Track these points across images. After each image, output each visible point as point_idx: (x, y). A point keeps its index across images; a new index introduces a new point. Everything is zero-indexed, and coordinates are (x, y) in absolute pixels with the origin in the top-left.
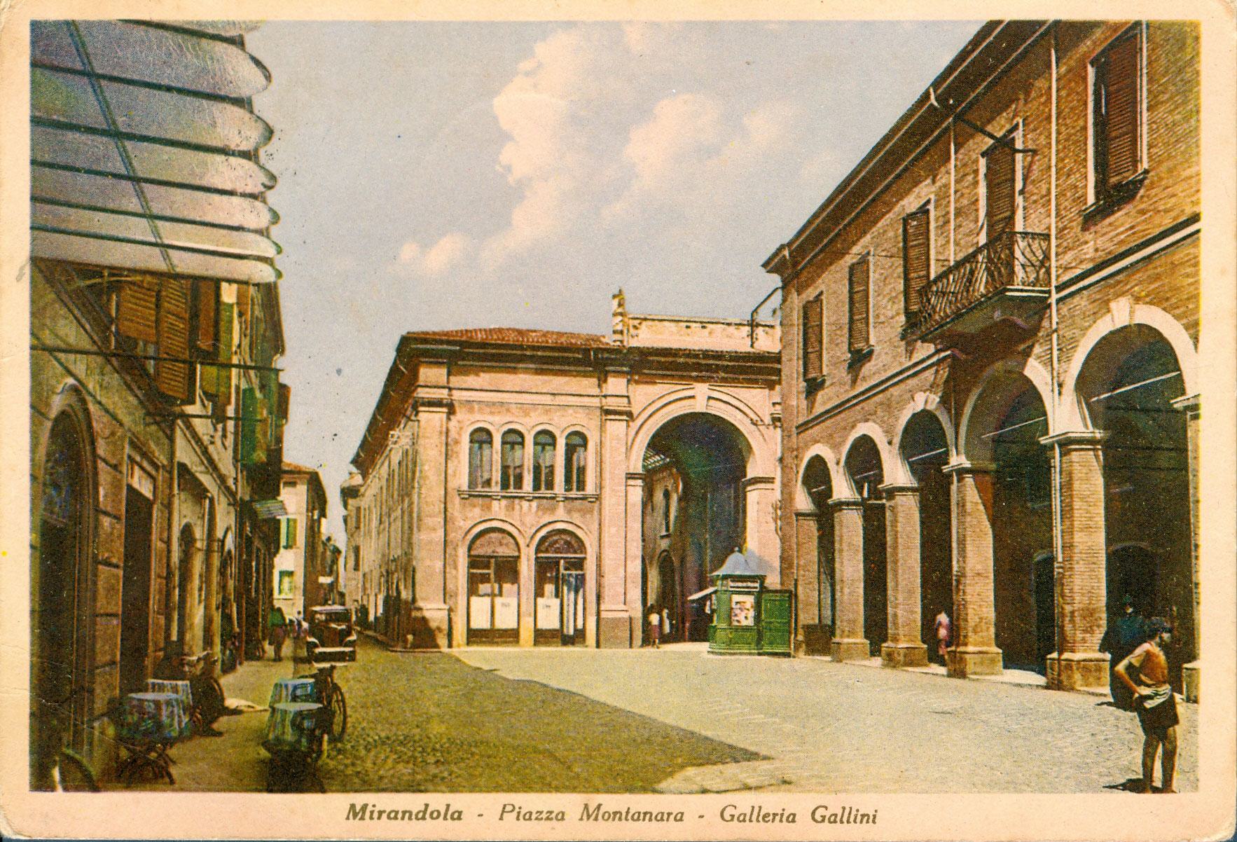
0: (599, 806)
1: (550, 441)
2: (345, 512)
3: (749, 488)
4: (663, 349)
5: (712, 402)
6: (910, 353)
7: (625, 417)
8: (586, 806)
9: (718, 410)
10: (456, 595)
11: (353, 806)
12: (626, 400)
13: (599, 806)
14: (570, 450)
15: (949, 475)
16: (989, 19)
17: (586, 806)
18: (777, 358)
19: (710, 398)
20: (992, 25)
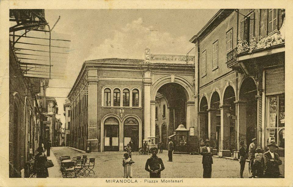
0: (164, 180)
1: (128, 92)
2: (64, 112)
3: (188, 105)
4: (18, 30)
5: (176, 80)
6: (20, 60)
7: (150, 85)
8: (161, 180)
9: (180, 82)
10: (152, 102)
11: (107, 181)
12: (150, 79)
13: (164, 180)
14: (134, 95)
15: (235, 104)
16: (221, 8)
17: (161, 180)
18: (47, 121)
19: (175, 78)
20: (222, 10)
